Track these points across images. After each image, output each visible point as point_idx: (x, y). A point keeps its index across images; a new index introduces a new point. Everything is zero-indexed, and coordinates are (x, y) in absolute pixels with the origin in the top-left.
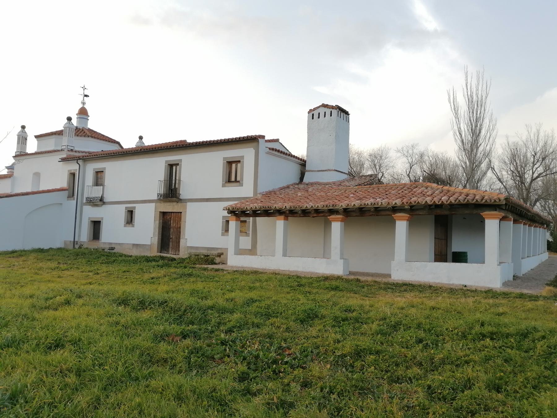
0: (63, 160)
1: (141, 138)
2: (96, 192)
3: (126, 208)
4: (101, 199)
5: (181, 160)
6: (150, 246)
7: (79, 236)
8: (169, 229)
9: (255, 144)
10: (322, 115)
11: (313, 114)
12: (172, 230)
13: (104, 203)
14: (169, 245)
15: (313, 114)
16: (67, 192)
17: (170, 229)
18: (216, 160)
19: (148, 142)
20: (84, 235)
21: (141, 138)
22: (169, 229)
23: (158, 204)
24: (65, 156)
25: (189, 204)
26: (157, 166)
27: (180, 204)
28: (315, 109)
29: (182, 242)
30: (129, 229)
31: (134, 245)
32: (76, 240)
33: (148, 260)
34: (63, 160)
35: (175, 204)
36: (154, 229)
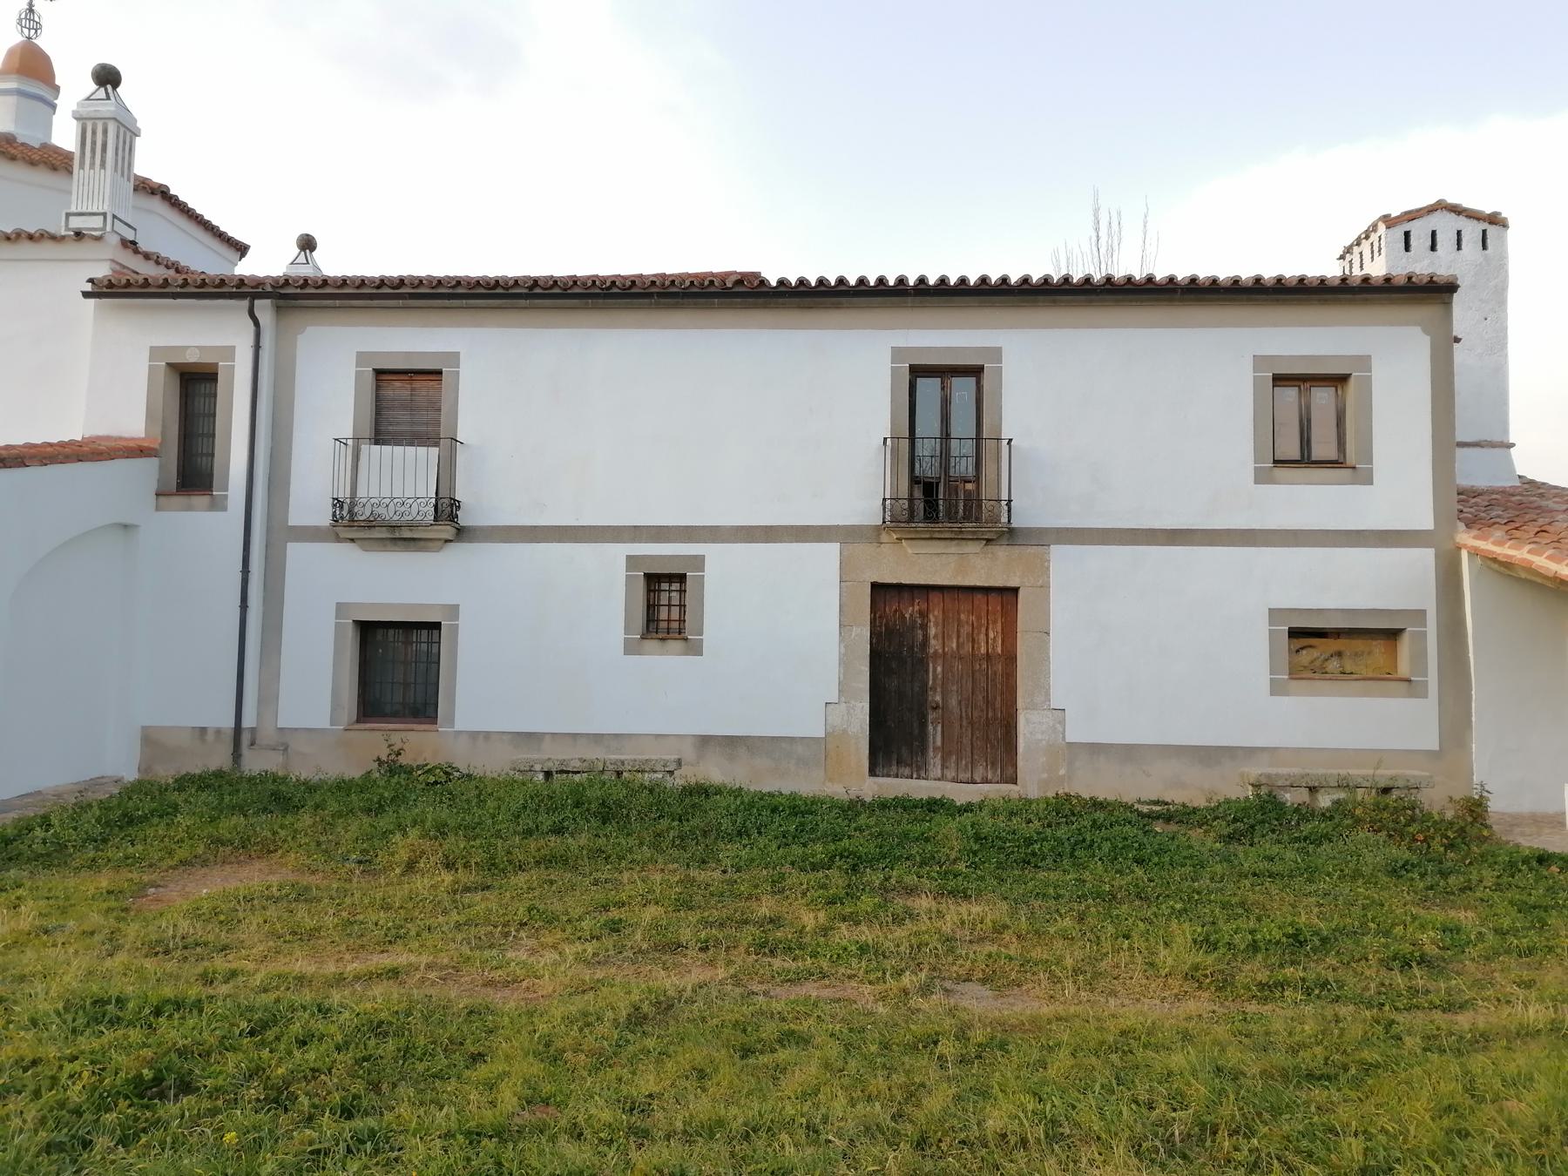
0: (103, 290)
1: (307, 244)
2: (401, 478)
3: (632, 561)
4: (447, 510)
5: (454, 358)
6: (823, 750)
7: (269, 697)
8: (933, 664)
9: (1428, 312)
10: (1446, 240)
11: (1407, 235)
12: (936, 670)
13: (462, 534)
14: (923, 737)
15: (1407, 235)
16: (149, 466)
17: (922, 663)
18: (1221, 368)
19: (332, 263)
20: (311, 692)
21: (307, 244)
22: (933, 664)
23: (863, 550)
24: (102, 271)
25: (1061, 558)
26: (858, 371)
27: (1001, 552)
28: (1411, 216)
29: (1030, 728)
30: (664, 663)
31: (705, 741)
32: (248, 721)
33: (793, 818)
34: (103, 290)
35: (972, 548)
36: (845, 662)
